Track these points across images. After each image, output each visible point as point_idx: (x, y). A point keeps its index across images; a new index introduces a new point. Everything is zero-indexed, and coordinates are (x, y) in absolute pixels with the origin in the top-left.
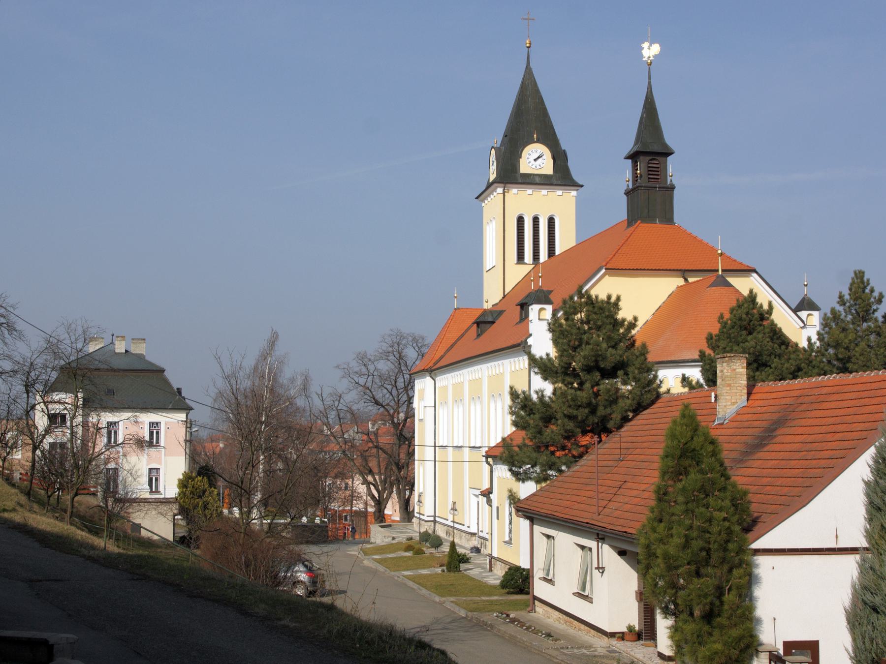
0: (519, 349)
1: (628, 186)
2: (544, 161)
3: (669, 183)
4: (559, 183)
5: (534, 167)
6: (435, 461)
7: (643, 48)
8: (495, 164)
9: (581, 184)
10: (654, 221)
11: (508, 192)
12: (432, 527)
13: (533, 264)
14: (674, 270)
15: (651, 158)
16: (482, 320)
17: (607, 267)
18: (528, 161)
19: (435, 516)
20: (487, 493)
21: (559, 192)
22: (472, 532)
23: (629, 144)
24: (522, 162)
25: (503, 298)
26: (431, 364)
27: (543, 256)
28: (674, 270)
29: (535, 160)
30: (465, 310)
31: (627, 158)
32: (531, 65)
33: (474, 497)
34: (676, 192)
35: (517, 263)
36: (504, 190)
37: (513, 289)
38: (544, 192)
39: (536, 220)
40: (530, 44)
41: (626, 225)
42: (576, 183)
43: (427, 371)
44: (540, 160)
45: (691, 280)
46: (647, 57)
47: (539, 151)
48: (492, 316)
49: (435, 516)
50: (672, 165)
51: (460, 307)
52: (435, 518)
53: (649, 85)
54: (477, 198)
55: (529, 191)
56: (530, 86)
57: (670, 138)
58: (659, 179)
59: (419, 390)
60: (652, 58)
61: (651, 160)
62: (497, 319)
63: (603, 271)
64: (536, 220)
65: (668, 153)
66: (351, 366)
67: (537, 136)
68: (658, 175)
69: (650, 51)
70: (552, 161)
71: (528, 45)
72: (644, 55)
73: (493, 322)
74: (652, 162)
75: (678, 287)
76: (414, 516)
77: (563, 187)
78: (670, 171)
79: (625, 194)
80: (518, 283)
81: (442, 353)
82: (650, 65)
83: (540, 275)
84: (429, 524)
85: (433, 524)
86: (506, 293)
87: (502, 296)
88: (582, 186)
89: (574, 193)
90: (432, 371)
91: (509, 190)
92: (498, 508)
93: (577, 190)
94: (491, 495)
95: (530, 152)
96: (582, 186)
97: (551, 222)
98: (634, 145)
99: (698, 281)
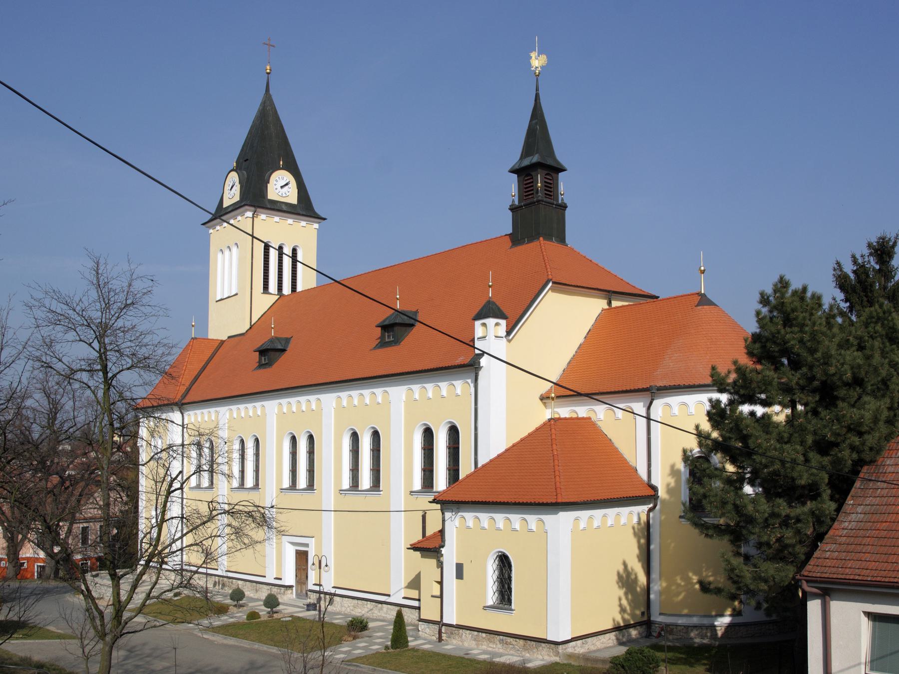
0: (471, 369)
1: (513, 201)
3: (560, 202)
4: (304, 213)
5: (280, 194)
9: (324, 217)
10: (551, 240)
11: (257, 217)
13: (278, 295)
15: (546, 172)
16: (272, 348)
21: (303, 223)
22: (286, 584)
23: (513, 154)
24: (270, 187)
25: (250, 328)
27: (287, 289)
29: (282, 187)
30: (202, 340)
32: (271, 92)
33: (290, 545)
34: (568, 212)
35: (263, 293)
36: (253, 214)
38: (290, 221)
40: (270, 70)
42: (319, 215)
43: (176, 404)
44: (287, 187)
45: (615, 304)
47: (285, 178)
51: (197, 337)
52: (182, 567)
55: (277, 219)
57: (562, 155)
65: (560, 169)
69: (537, 62)
71: (268, 71)
73: (283, 350)
78: (562, 188)
79: (510, 209)
83: (490, 284)
86: (252, 323)
87: (248, 327)
88: (325, 219)
89: (316, 226)
90: (183, 404)
91: (257, 215)
93: (319, 223)
95: (277, 179)
96: (325, 219)
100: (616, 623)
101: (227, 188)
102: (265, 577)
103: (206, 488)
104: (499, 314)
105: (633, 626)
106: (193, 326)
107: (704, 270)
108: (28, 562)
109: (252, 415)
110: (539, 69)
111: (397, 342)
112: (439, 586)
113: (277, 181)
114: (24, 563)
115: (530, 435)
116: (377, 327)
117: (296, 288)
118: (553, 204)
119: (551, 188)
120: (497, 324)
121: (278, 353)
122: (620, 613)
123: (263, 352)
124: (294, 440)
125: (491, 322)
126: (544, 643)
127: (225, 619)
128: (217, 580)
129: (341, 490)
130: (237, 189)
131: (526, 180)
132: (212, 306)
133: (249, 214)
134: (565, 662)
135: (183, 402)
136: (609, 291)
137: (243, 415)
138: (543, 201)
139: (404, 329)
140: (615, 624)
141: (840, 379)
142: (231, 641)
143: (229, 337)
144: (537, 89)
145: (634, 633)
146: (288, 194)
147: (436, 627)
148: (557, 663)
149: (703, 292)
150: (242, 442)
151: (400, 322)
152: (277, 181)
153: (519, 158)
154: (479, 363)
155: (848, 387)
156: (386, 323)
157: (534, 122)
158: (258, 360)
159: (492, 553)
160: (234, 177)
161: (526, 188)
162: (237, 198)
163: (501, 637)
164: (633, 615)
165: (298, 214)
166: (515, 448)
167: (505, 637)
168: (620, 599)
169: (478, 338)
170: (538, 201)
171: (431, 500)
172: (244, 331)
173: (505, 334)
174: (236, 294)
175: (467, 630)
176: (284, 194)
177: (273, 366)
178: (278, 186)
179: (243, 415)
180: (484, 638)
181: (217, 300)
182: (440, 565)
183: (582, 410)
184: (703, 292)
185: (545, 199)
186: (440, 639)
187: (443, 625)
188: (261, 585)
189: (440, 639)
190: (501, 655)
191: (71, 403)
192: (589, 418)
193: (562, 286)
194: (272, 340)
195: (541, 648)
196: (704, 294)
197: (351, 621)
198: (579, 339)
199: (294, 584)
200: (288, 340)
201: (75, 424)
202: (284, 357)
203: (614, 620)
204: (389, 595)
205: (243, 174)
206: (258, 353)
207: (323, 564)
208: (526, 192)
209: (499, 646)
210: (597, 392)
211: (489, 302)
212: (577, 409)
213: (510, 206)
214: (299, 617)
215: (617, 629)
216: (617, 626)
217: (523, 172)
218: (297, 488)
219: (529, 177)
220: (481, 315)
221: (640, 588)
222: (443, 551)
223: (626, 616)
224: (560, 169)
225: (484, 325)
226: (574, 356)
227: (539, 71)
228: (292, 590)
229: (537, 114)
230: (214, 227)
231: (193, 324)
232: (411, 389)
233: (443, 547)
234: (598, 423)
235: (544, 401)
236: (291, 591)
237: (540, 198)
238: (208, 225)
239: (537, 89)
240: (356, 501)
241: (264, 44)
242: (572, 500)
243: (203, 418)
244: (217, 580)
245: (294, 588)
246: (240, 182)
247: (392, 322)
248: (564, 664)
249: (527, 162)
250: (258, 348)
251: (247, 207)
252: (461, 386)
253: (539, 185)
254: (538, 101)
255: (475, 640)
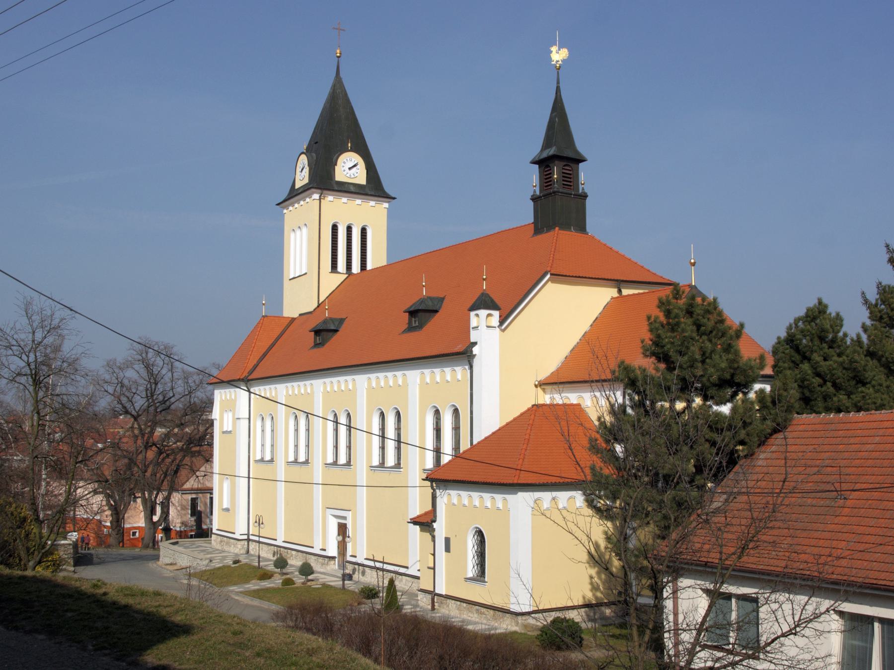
1: (535, 191)
2: (357, 171)
3: (580, 191)
4: (373, 193)
5: (348, 175)
6: (249, 478)
7: (552, 52)
8: (306, 170)
9: (393, 196)
10: (568, 229)
11: (324, 199)
12: (246, 546)
13: (346, 274)
14: (608, 280)
15: (565, 163)
17: (552, 273)
18: (343, 169)
19: (248, 535)
20: (430, 522)
21: (372, 203)
22: (330, 555)
23: (535, 147)
25: (318, 306)
26: (245, 374)
27: (356, 268)
28: (608, 280)
29: (350, 169)
31: (534, 162)
32: (342, 75)
33: (332, 517)
34: (588, 202)
35: (331, 272)
36: (320, 196)
37: (330, 294)
38: (359, 201)
39: (349, 229)
40: (340, 54)
41: (533, 232)
42: (389, 195)
44: (355, 169)
45: (625, 292)
46: (555, 61)
47: (353, 160)
48: (334, 324)
49: (248, 535)
50: (584, 174)
51: (268, 315)
52: (248, 536)
53: (558, 90)
54: (278, 204)
55: (344, 200)
56: (341, 95)
57: (582, 145)
58: (571, 186)
59: (222, 401)
60: (560, 62)
61: (565, 166)
62: (340, 328)
63: (548, 276)
64: (349, 229)
65: (579, 160)
66: (100, 373)
67: (351, 145)
68: (570, 182)
69: (558, 55)
70: (366, 171)
71: (338, 55)
72: (553, 59)
73: (336, 331)
74: (566, 168)
75: (612, 298)
76: (212, 533)
77: (376, 198)
78: (582, 177)
80: (332, 292)
81: (255, 362)
82: (559, 69)
83: (485, 277)
84: (243, 542)
85: (246, 543)
86: (320, 302)
87: (316, 305)
88: (394, 198)
89: (386, 205)
90: (249, 380)
91: (325, 197)
92: (447, 540)
93: (389, 202)
94: (433, 524)
95: (346, 161)
96: (394, 198)
97: (364, 231)
98: (542, 150)
99: (634, 295)
100: (586, 600)
101: (299, 170)
102: (313, 547)
103: (267, 461)
104: (495, 307)
105: (607, 605)
106: (263, 304)
107: (695, 263)
108: (139, 532)
109: (351, 389)
110: (560, 62)
111: (420, 327)
112: (432, 557)
113: (344, 163)
114: (136, 532)
115: (515, 419)
116: (310, 331)
117: (366, 267)
118: (571, 194)
119: (570, 179)
120: (489, 315)
121: (331, 334)
122: (591, 590)
123: (317, 332)
124: (382, 415)
125: (483, 313)
126: (508, 613)
127: (266, 584)
128: (276, 550)
129: (371, 467)
130: (306, 171)
131: (546, 171)
132: (287, 284)
133: (316, 196)
134: (523, 632)
135: (250, 377)
136: (617, 281)
137: (391, 383)
138: (559, 192)
139: (427, 314)
140: (585, 601)
141: (708, 380)
142: (256, 602)
143: (300, 315)
144: (558, 82)
145: (608, 611)
146: (356, 175)
147: (429, 596)
148: (515, 632)
149: (693, 284)
150: (437, 412)
151: (424, 308)
152: (344, 163)
153: (540, 149)
154: (472, 351)
155: (717, 388)
156: (412, 309)
157: (554, 114)
158: (407, 322)
159: (471, 528)
160: (304, 159)
161: (546, 180)
162: (306, 181)
163: (477, 607)
164: (606, 595)
165: (366, 194)
166: (501, 431)
167: (480, 608)
168: (591, 577)
169: (473, 328)
170: (554, 192)
171: (424, 478)
172: (312, 309)
173: (499, 324)
174: (306, 274)
175: (453, 600)
176: (352, 175)
177: (424, 328)
178: (346, 168)
179: (391, 383)
180: (465, 608)
181: (291, 278)
182: (433, 537)
183: (572, 397)
184: (693, 284)
185: (561, 190)
186: (433, 608)
187: (435, 595)
188: (310, 556)
189: (433, 608)
190: (476, 623)
191: (170, 374)
192: (579, 405)
193: (560, 277)
194: (325, 321)
195: (505, 618)
196: (695, 285)
197: (362, 589)
198: (585, 326)
199: (337, 556)
200: (342, 321)
201: (174, 396)
202: (336, 337)
203: (584, 598)
204: (407, 568)
205: (312, 157)
206: (313, 333)
207: (261, 522)
208: (546, 183)
209: (476, 615)
210: (582, 380)
211: (483, 294)
212: (569, 395)
213: (532, 196)
214: (329, 585)
215: (587, 605)
216: (587, 603)
217: (544, 163)
218: (385, 466)
219: (548, 169)
220: (474, 308)
221: (616, 568)
222: (435, 525)
223: (599, 594)
224: (579, 160)
225: (477, 315)
226: (578, 343)
227: (560, 64)
228: (335, 561)
229: (558, 109)
230: (287, 207)
231: (264, 302)
232: (433, 372)
233: (435, 521)
234: (586, 409)
235: (542, 387)
236: (333, 562)
237: (555, 189)
238: (282, 205)
239: (558, 82)
240: (384, 477)
241: (334, 28)
242: (529, 482)
243: (299, 390)
244: (276, 550)
245: (337, 559)
246: (308, 165)
247: (417, 308)
248: (521, 633)
249: (545, 155)
250: (314, 328)
251: (313, 190)
252: (460, 372)
253: (555, 176)
254: (558, 94)
255: (458, 609)
